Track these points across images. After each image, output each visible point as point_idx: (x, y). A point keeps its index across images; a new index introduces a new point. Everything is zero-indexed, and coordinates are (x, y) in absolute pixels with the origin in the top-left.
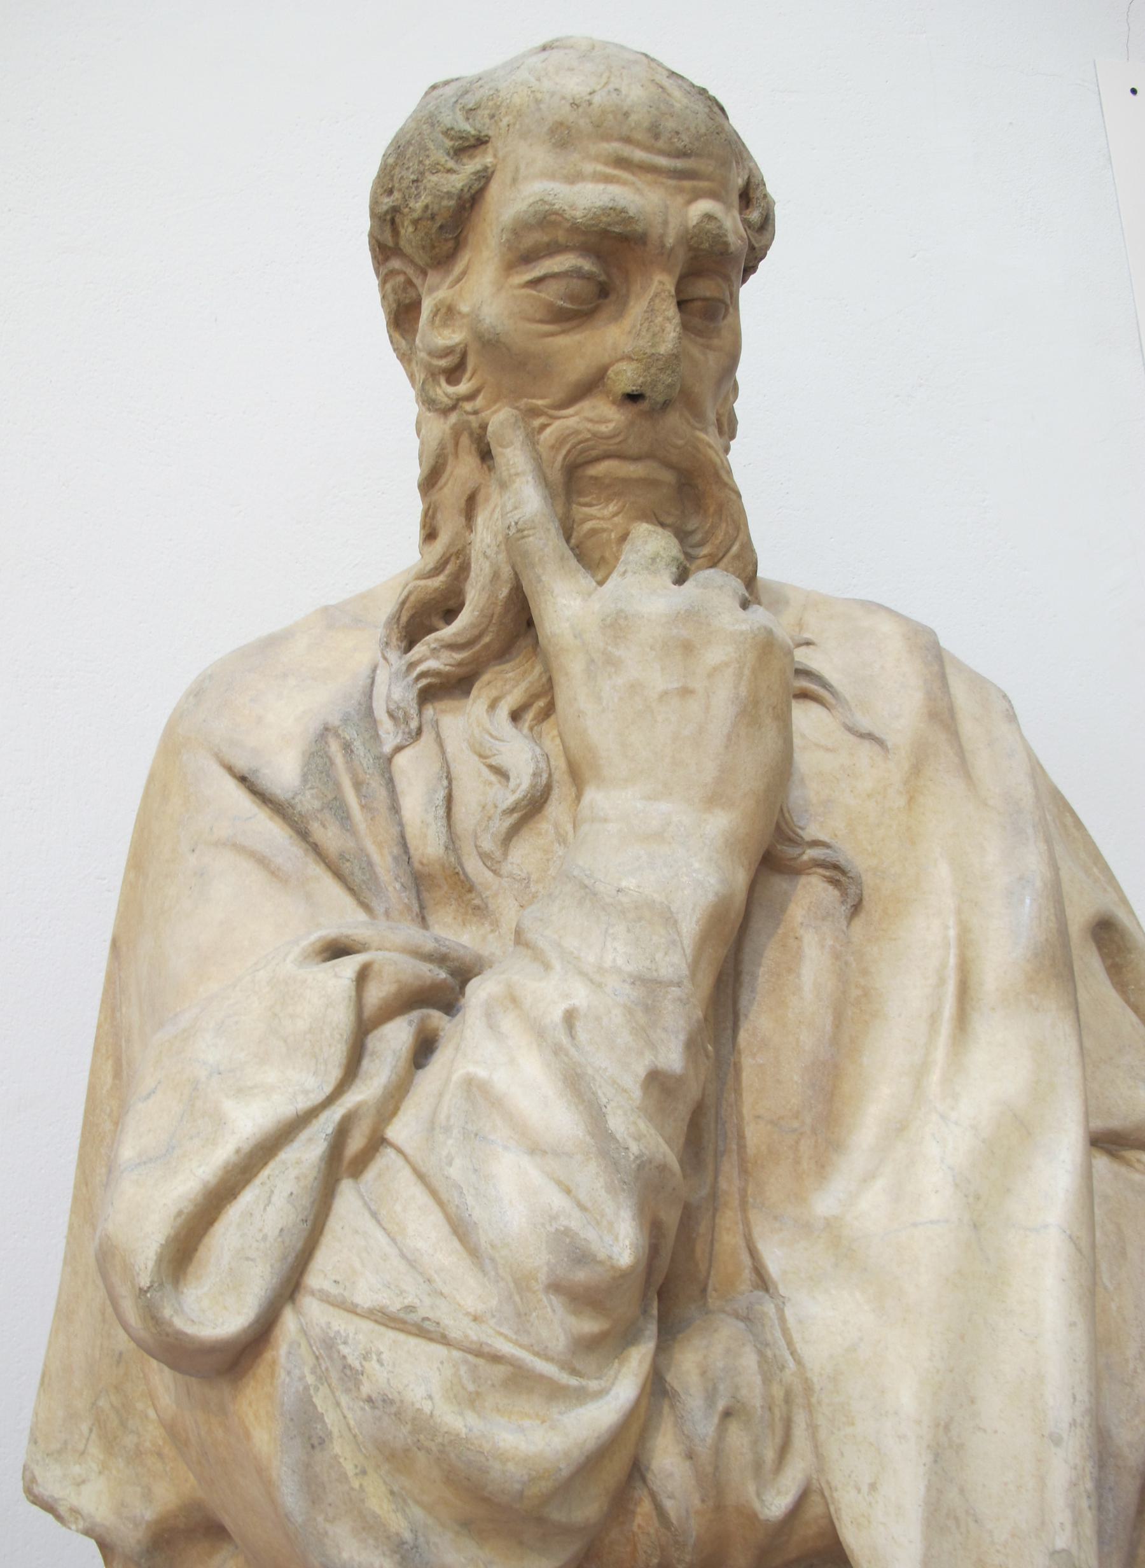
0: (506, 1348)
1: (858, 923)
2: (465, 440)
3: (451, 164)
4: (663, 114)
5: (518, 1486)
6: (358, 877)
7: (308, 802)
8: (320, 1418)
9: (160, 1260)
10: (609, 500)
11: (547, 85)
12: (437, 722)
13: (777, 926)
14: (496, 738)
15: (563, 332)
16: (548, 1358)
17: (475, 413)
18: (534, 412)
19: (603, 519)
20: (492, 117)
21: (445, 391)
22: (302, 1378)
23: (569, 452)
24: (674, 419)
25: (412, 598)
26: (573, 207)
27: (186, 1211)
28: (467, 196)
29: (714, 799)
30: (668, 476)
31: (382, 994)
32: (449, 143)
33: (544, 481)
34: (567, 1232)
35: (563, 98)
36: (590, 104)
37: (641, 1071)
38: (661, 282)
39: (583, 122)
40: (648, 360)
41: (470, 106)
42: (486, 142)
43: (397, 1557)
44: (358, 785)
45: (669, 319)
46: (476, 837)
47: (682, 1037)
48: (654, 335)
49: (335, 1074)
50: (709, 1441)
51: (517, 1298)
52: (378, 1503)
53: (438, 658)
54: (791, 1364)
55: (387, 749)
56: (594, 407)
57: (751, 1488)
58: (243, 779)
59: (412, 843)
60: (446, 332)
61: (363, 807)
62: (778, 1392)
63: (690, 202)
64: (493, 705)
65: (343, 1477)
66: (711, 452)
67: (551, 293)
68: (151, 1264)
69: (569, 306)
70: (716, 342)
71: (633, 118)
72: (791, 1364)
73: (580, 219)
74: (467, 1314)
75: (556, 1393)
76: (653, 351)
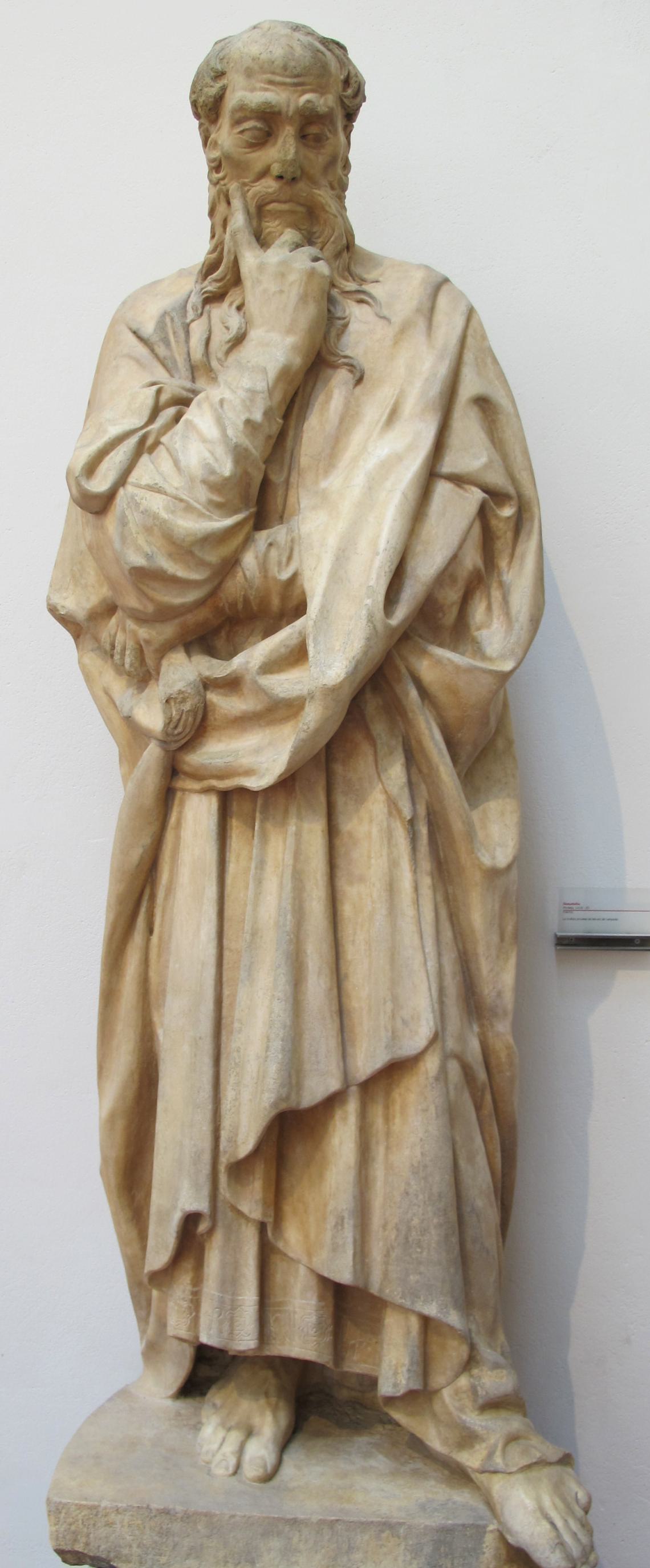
0: (184, 497)
1: (359, 388)
2: (222, 196)
3: (212, 84)
4: (290, 60)
5: (183, 537)
6: (170, 365)
7: (155, 339)
8: (127, 517)
9: (82, 469)
10: (276, 219)
11: (246, 50)
12: (210, 311)
13: (326, 386)
14: (229, 316)
15: (253, 151)
16: (200, 504)
17: (225, 185)
18: (244, 184)
19: (272, 227)
20: (228, 63)
21: (216, 176)
22: (123, 506)
23: (258, 200)
24: (301, 185)
25: (206, 263)
26: (251, 102)
27: (92, 455)
28: (217, 97)
29: (289, 331)
30: (300, 209)
31: (166, 398)
32: (213, 74)
33: (248, 212)
34: (208, 464)
35: (250, 57)
36: (259, 59)
37: (243, 418)
38: (289, 130)
39: (256, 67)
40: (283, 162)
41: (221, 58)
42: (225, 74)
43: (146, 559)
44: (174, 333)
45: (291, 145)
46: (216, 353)
47: (262, 411)
48: (286, 152)
49: (145, 419)
50: (262, 552)
51: (190, 483)
52: (141, 541)
53: (211, 285)
54: (297, 531)
55: (188, 321)
56: (266, 182)
57: (276, 569)
58: (135, 333)
59: (192, 354)
60: (214, 152)
61: (175, 341)
62: (289, 538)
63: (300, 96)
64: (231, 304)
65: (132, 534)
66: (320, 198)
67: (247, 136)
68: (79, 469)
69: (253, 141)
70: (323, 151)
71: (276, 63)
72: (297, 531)
74: (174, 487)
75: (201, 515)
76: (285, 158)
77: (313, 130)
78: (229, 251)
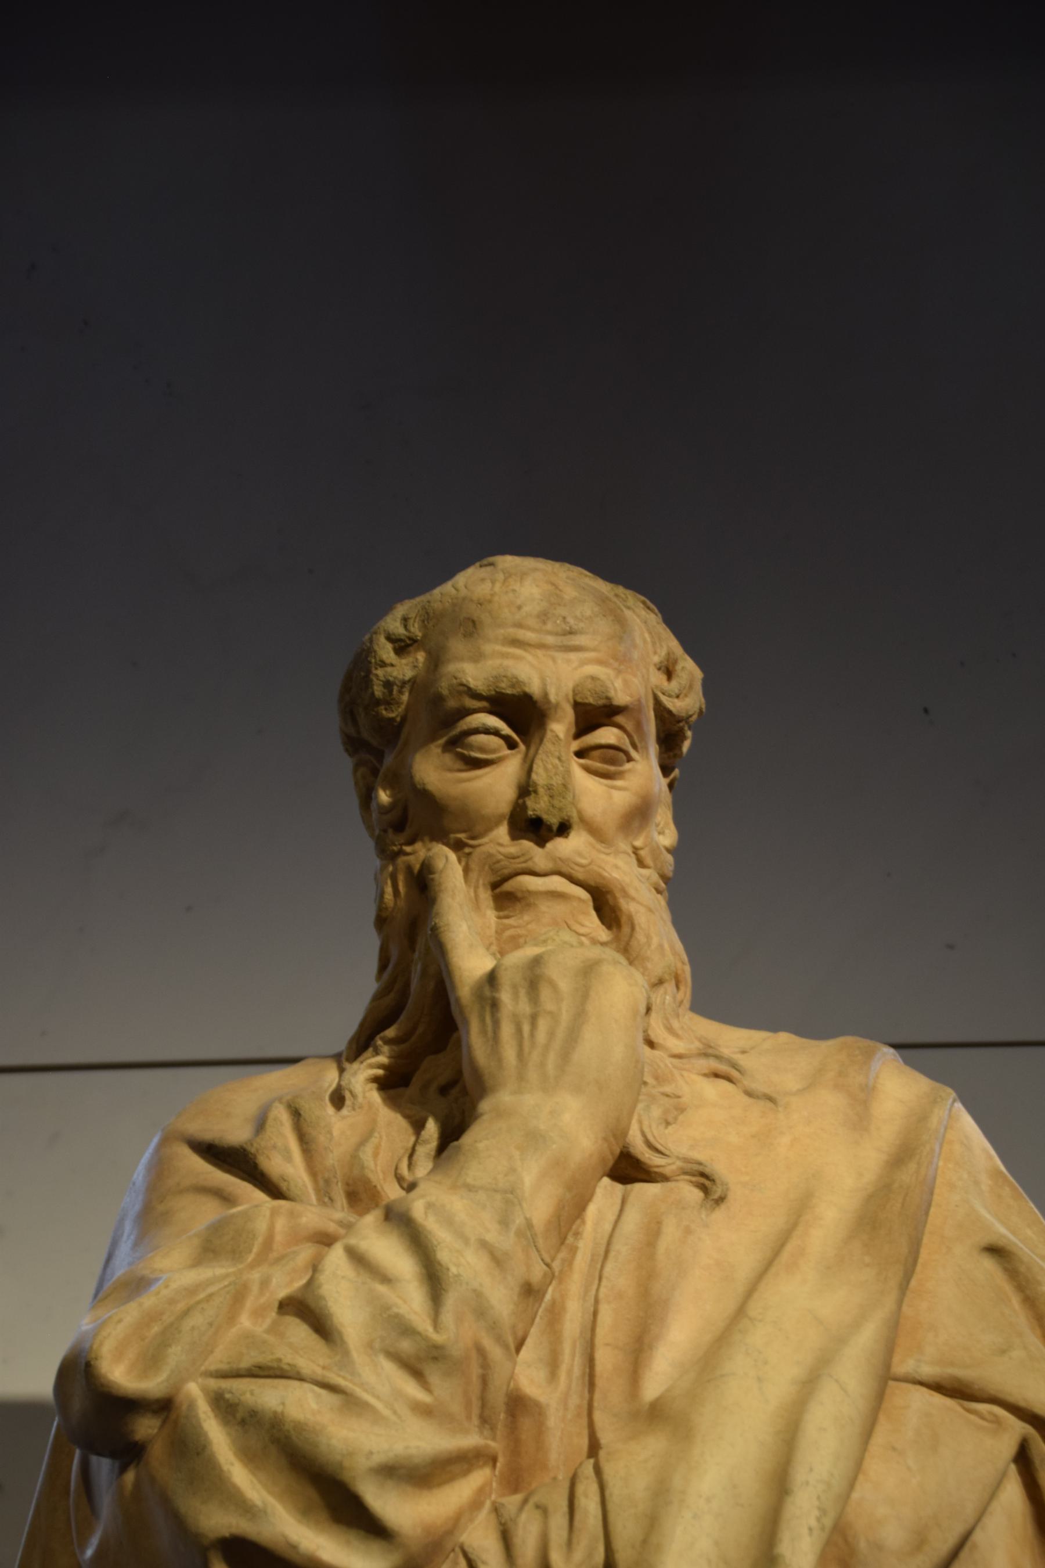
46: (553, 806)
77: (607, 735)
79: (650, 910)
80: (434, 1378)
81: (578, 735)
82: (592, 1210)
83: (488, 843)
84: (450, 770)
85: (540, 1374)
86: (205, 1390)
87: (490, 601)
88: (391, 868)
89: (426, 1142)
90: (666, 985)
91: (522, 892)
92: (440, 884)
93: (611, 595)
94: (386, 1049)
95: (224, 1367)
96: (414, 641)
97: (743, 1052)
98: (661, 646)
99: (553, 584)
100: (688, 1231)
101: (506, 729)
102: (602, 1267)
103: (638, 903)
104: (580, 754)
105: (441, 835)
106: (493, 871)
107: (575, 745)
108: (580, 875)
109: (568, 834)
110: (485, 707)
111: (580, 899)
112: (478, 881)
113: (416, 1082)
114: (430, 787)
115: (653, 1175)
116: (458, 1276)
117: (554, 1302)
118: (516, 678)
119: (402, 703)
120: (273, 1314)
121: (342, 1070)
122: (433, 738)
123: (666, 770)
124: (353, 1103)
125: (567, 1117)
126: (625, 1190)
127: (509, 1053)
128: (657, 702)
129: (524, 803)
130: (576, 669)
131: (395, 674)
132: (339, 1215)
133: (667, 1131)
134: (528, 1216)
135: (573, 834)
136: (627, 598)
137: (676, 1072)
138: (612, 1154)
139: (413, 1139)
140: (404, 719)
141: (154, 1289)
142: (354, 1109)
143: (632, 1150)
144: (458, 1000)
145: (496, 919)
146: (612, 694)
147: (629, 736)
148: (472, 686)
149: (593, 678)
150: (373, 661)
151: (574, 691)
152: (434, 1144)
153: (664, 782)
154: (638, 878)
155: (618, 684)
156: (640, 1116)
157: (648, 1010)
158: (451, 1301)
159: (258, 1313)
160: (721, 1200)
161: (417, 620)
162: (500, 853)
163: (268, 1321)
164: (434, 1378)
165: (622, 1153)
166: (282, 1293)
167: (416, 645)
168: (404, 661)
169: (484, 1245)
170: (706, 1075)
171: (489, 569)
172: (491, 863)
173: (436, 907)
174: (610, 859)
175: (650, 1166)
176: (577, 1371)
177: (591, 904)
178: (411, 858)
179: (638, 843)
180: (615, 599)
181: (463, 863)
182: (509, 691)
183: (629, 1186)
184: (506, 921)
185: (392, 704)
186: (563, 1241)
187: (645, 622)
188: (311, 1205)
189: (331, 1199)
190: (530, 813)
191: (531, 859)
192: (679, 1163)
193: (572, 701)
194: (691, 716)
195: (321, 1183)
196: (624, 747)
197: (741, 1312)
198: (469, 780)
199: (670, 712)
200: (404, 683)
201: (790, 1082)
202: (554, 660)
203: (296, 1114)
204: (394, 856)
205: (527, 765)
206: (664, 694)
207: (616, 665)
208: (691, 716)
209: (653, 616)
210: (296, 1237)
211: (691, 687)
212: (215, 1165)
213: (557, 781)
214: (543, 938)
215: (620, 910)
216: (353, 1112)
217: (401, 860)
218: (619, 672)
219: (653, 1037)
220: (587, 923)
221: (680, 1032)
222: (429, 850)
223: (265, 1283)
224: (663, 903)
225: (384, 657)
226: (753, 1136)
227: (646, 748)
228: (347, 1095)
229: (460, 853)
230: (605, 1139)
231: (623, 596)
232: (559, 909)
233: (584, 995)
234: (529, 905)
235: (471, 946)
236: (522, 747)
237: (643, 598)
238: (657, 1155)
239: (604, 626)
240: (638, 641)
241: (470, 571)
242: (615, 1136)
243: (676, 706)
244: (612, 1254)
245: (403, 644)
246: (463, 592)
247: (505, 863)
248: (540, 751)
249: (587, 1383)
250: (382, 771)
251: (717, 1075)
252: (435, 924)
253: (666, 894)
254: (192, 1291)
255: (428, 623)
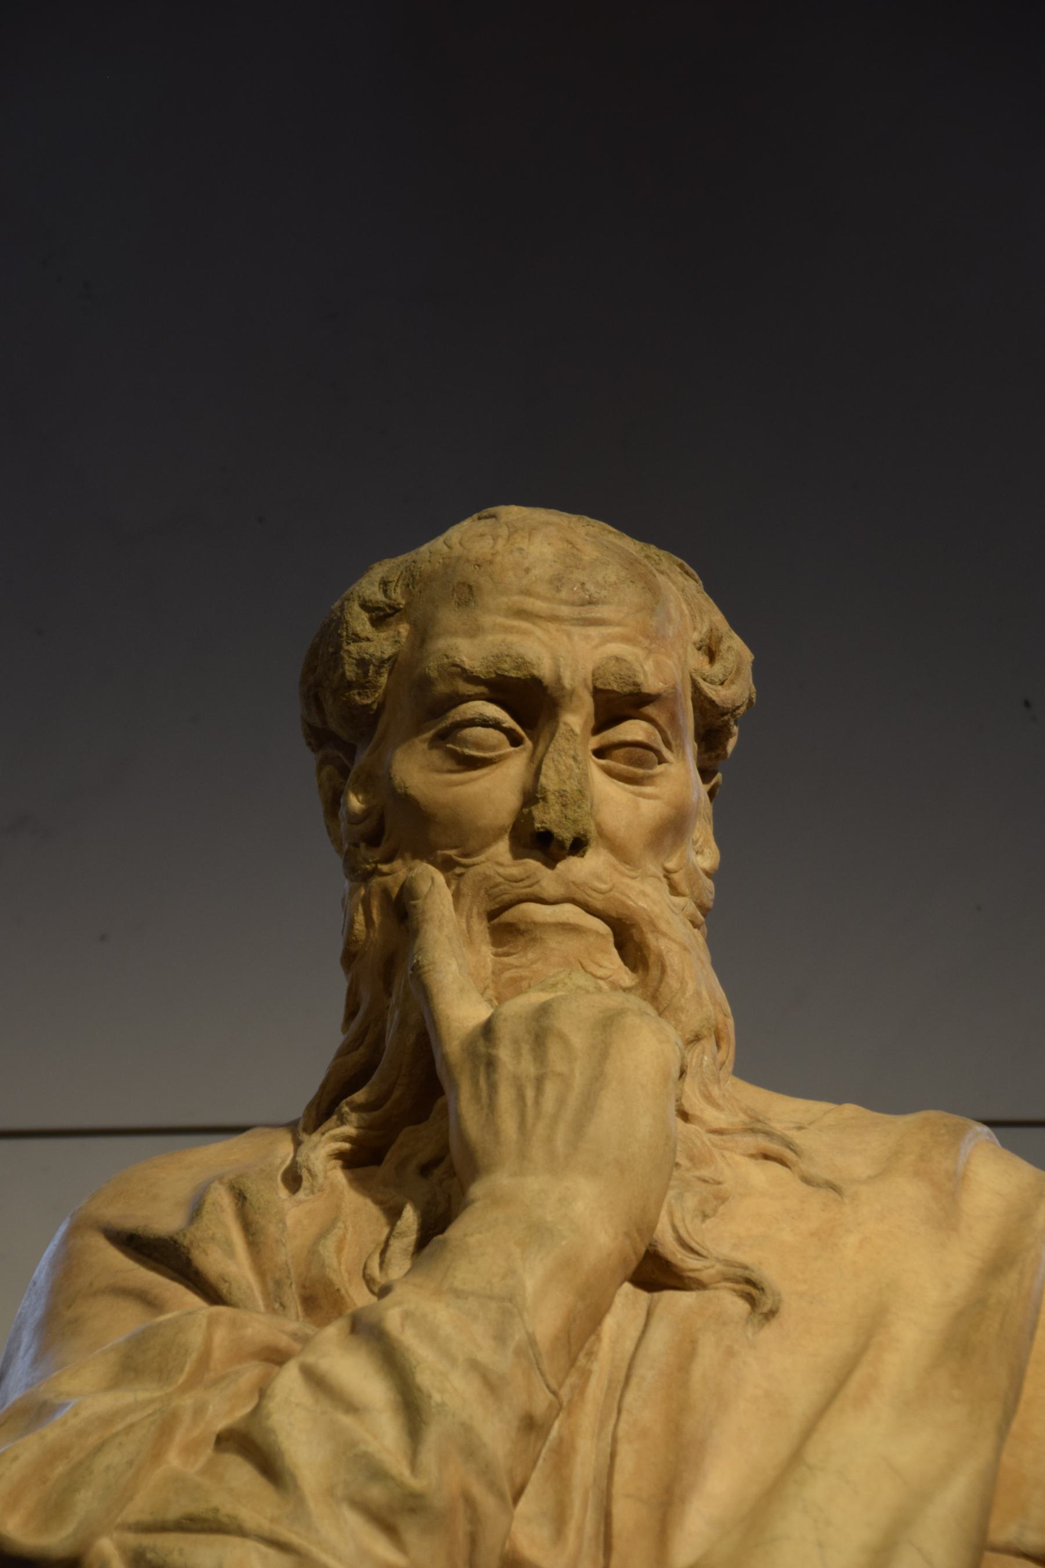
73: (478, 667)
77: (634, 730)
78: (402, 1023)
79: (685, 949)
80: (411, 1535)
81: (597, 730)
82: (609, 1323)
83: (483, 862)
84: (439, 771)
85: (543, 1532)
86: (122, 1549)
87: (491, 562)
88: (363, 892)
89: (403, 1235)
90: (703, 1042)
91: (526, 923)
92: (424, 912)
93: (640, 556)
94: (353, 1117)
95: (146, 1518)
96: (396, 609)
97: (800, 1128)
98: (702, 620)
99: (569, 542)
100: (730, 1353)
101: (509, 722)
102: (622, 1396)
103: (670, 939)
104: (600, 753)
105: (425, 852)
106: (491, 897)
107: (594, 742)
108: (598, 903)
109: (584, 852)
110: (482, 694)
111: (598, 934)
112: (471, 909)
113: (391, 1158)
114: (412, 792)
115: (687, 1281)
116: (443, 1404)
117: (560, 1440)
118: (522, 658)
119: (380, 687)
120: (209, 1451)
121: (298, 1144)
122: (418, 731)
123: (706, 774)
124: (312, 1185)
125: (580, 1206)
126: (652, 1300)
127: (509, 1125)
128: (697, 690)
129: (530, 812)
130: (596, 647)
131: (371, 650)
132: (293, 1326)
133: (704, 1226)
134: (530, 1330)
135: (590, 853)
136: (660, 560)
137: (716, 1152)
138: (636, 1253)
139: (386, 1231)
140: (382, 706)
141: (59, 1417)
142: (313, 1192)
143: (660, 1249)
144: (444, 1056)
145: (492, 957)
146: (641, 679)
147: (661, 731)
148: (467, 667)
149: (618, 659)
150: (345, 634)
151: (593, 675)
152: (412, 1237)
153: (704, 789)
154: (669, 907)
155: (649, 666)
156: (670, 1205)
157: (682, 1073)
158: (432, 1436)
159: (190, 1449)
160: (771, 1314)
161: (399, 584)
162: (499, 875)
163: (202, 1460)
164: (411, 1535)
165: (647, 1252)
166: (221, 1425)
167: (397, 614)
168: (382, 635)
169: (474, 1365)
170: (752, 1156)
171: (489, 521)
172: (488, 887)
173: (418, 941)
174: (636, 884)
175: (683, 1270)
176: (589, 1529)
177: (611, 939)
178: (388, 878)
179: (671, 865)
180: (645, 561)
181: (453, 887)
182: (513, 674)
183: (656, 1295)
184: (506, 959)
185: (367, 688)
186: (573, 1361)
187: (683, 591)
188: (259, 1312)
189: (282, 1305)
190: (538, 825)
191: (538, 882)
192: (719, 1267)
193: (591, 687)
194: (738, 708)
195: (271, 1285)
196: (655, 745)
197: (796, 1457)
198: (462, 783)
199: (712, 702)
200: (383, 662)
201: (859, 1166)
202: (569, 636)
203: (240, 1197)
204: (366, 877)
205: (534, 766)
206: (705, 680)
207: (646, 643)
208: (738, 708)
209: (692, 582)
210: (239, 1354)
211: (738, 671)
212: (138, 1260)
213: (571, 786)
214: (551, 981)
215: (648, 947)
216: (312, 1196)
217: (376, 881)
218: (650, 652)
219: (687, 1107)
220: (606, 963)
221: (721, 1102)
222: (411, 869)
223: (199, 1411)
224: (701, 940)
225: (359, 629)
226: (812, 1234)
227: (682, 746)
228: (305, 1174)
229: (449, 874)
230: (627, 1235)
231: (656, 558)
232: (572, 945)
233: (602, 1053)
234: (534, 940)
235: (462, 990)
236: (528, 743)
237: (680, 561)
238: (692, 1256)
239: (632, 595)
240: (674, 614)
241: (466, 523)
242: (639, 1231)
243: (718, 694)
244: (634, 1381)
245: (382, 614)
246: (458, 550)
247: (505, 887)
248: (551, 749)
249: (602, 1545)
250: (355, 769)
251: (766, 1157)
252: (418, 962)
253: (704, 928)
254: (107, 1420)
255: (414, 588)
